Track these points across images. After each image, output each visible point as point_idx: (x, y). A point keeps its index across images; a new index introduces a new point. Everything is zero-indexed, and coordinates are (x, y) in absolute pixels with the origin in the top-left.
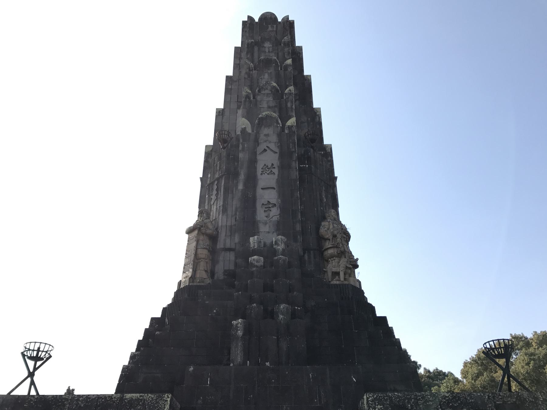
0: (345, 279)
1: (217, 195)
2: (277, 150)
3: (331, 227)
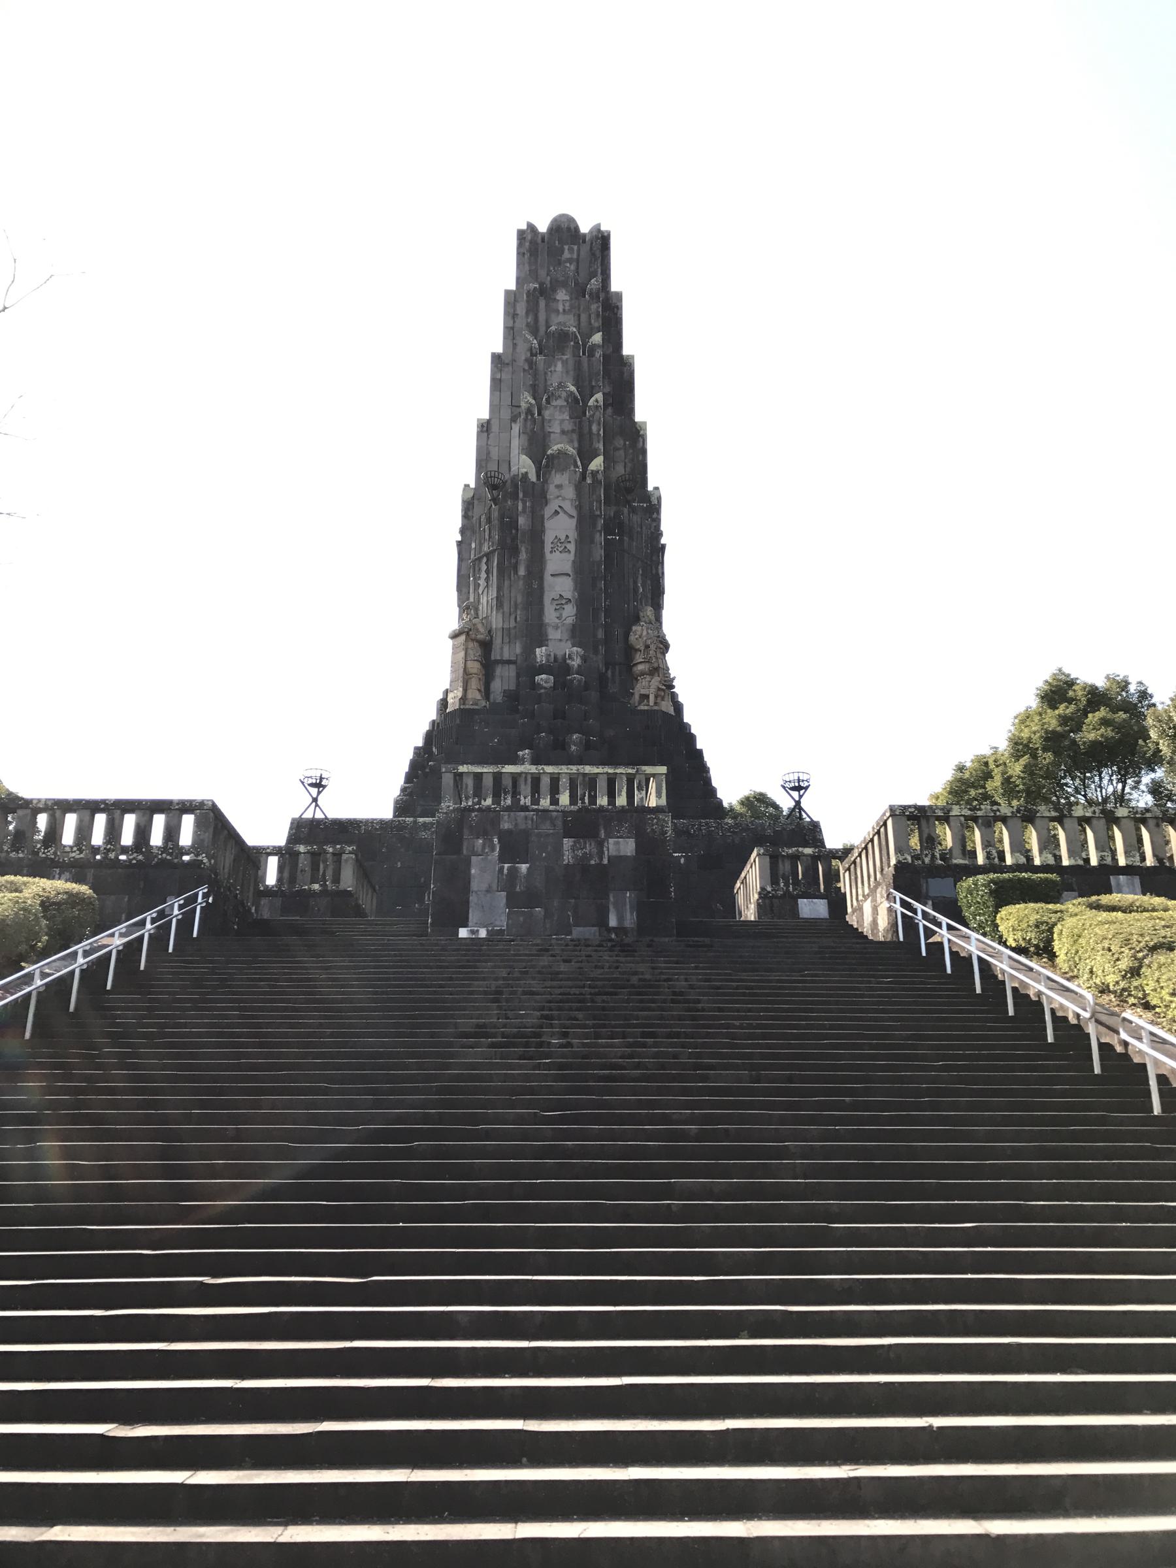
0: (656, 703)
1: (487, 580)
2: (574, 513)
3: (645, 633)
